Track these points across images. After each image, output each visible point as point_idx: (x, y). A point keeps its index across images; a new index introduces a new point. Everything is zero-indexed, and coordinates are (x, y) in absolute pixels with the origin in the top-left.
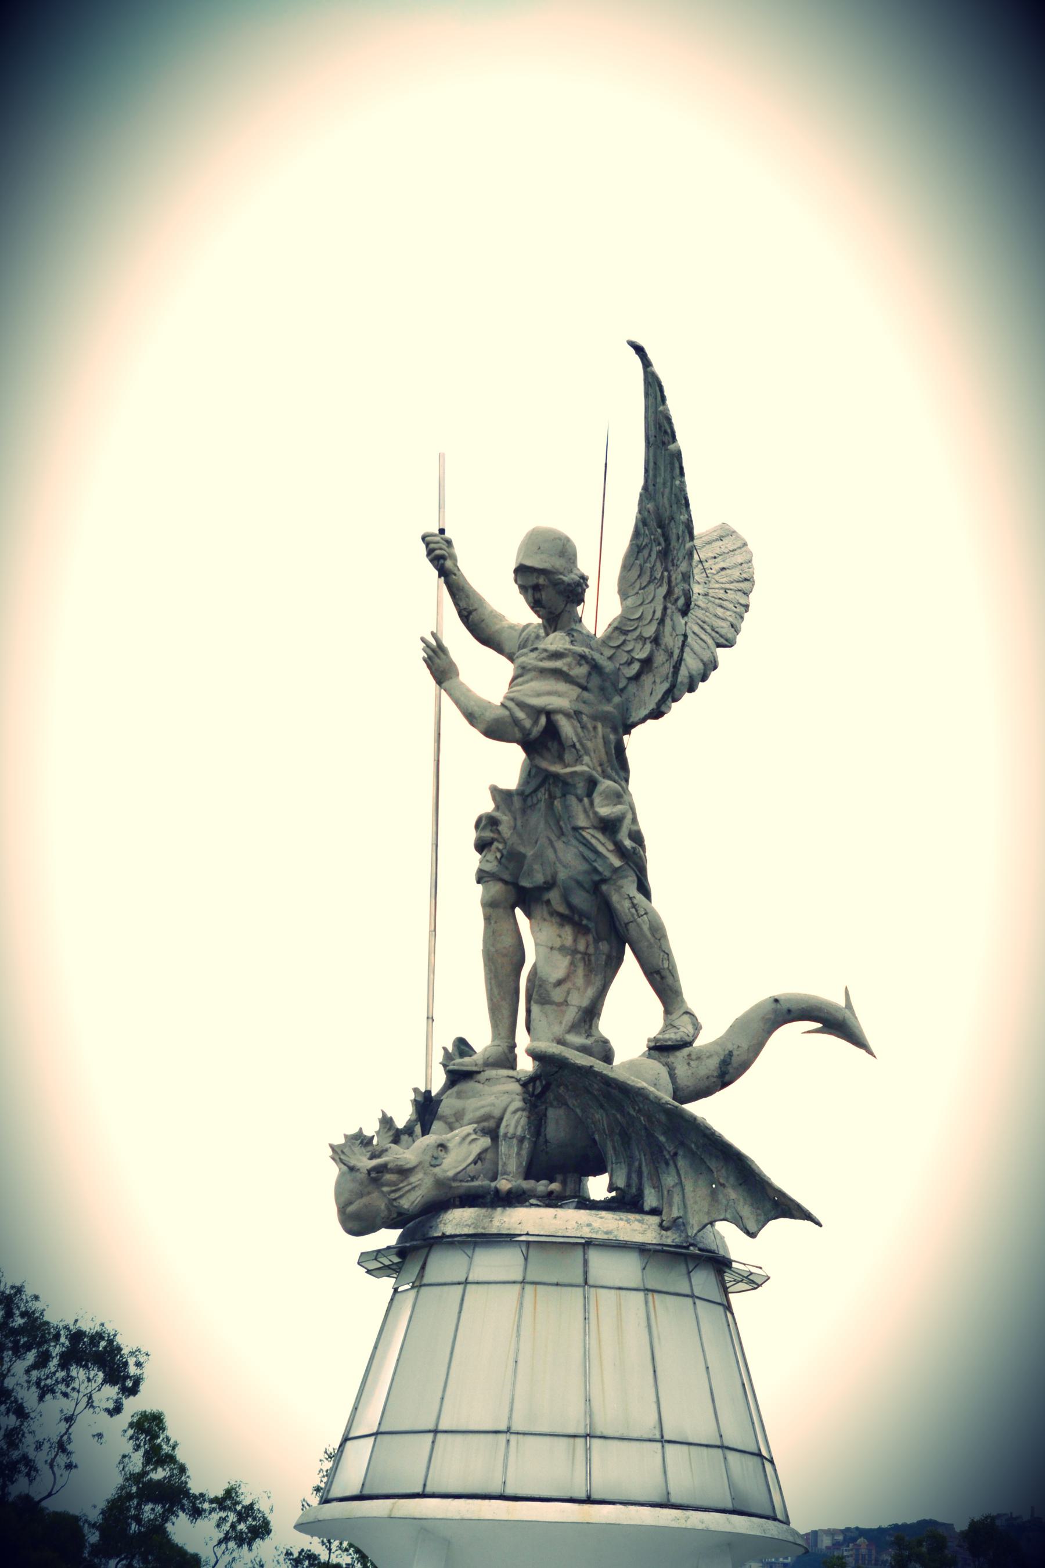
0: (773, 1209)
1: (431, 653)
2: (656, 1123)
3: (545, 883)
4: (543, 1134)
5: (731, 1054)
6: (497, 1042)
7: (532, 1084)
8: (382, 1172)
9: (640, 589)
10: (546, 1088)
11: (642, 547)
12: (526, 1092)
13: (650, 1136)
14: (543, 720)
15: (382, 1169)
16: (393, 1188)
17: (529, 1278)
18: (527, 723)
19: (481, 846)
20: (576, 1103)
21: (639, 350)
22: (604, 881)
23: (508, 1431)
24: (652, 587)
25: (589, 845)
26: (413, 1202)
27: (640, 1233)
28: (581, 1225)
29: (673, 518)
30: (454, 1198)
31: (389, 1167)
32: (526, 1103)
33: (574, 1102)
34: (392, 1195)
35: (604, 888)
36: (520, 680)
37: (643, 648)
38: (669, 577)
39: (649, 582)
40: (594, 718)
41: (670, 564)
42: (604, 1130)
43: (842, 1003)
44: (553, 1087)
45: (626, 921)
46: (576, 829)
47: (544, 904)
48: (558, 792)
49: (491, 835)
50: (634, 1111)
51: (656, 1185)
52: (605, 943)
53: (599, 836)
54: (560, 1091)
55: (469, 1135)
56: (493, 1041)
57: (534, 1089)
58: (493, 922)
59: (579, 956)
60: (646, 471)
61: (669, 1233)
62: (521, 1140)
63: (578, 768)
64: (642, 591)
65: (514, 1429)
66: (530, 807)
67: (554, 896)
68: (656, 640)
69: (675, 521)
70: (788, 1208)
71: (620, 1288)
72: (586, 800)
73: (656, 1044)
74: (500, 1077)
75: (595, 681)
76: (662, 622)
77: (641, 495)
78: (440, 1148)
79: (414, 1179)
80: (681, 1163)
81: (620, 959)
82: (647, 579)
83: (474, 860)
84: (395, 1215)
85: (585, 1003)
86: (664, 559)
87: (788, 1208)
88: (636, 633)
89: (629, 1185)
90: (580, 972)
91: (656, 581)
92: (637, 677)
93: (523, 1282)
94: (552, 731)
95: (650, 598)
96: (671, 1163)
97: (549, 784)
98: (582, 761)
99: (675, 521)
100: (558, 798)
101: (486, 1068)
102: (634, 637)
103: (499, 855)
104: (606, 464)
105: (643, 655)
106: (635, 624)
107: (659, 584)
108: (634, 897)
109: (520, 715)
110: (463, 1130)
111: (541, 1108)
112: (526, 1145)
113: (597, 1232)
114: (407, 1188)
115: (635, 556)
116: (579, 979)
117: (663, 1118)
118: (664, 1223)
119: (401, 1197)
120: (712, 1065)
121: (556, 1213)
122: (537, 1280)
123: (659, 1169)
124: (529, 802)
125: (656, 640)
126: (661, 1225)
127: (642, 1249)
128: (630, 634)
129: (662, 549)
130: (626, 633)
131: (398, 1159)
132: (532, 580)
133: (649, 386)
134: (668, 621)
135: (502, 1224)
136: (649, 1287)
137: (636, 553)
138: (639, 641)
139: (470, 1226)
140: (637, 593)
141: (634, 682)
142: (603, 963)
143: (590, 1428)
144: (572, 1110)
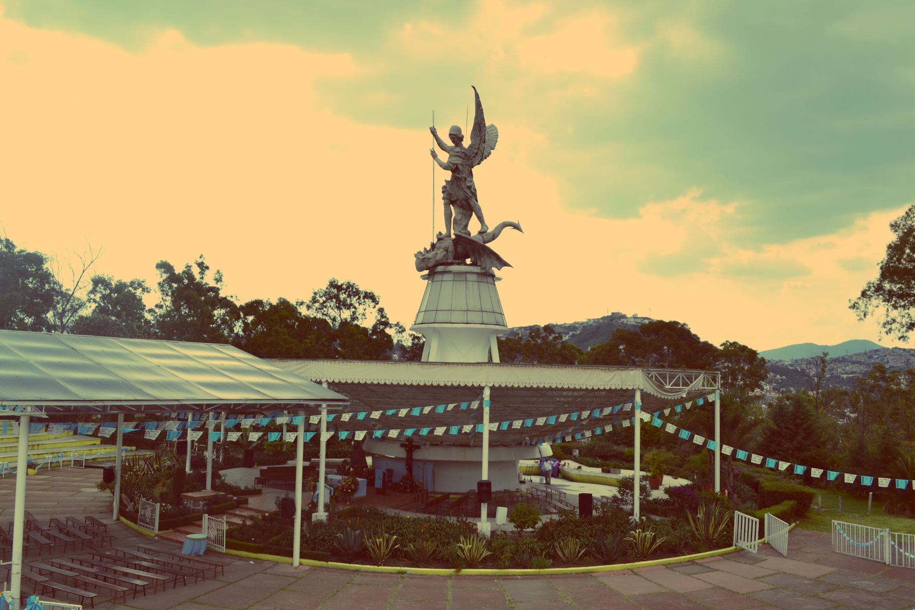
5: (495, 234)
10: (457, 242)
14: (455, 166)
15: (424, 258)
18: (452, 167)
21: (474, 88)
22: (468, 199)
23: (451, 310)
40: (466, 165)
46: (463, 188)
62: (453, 252)
63: (463, 176)
65: (453, 309)
67: (458, 202)
68: (478, 149)
70: (506, 264)
75: (466, 157)
76: (479, 145)
79: (431, 260)
81: (472, 215)
85: (465, 224)
87: (506, 264)
90: (464, 217)
92: (474, 156)
93: (454, 281)
94: (457, 168)
109: (450, 165)
112: (453, 254)
116: (464, 219)
120: (491, 235)
125: (478, 149)
127: (477, 273)
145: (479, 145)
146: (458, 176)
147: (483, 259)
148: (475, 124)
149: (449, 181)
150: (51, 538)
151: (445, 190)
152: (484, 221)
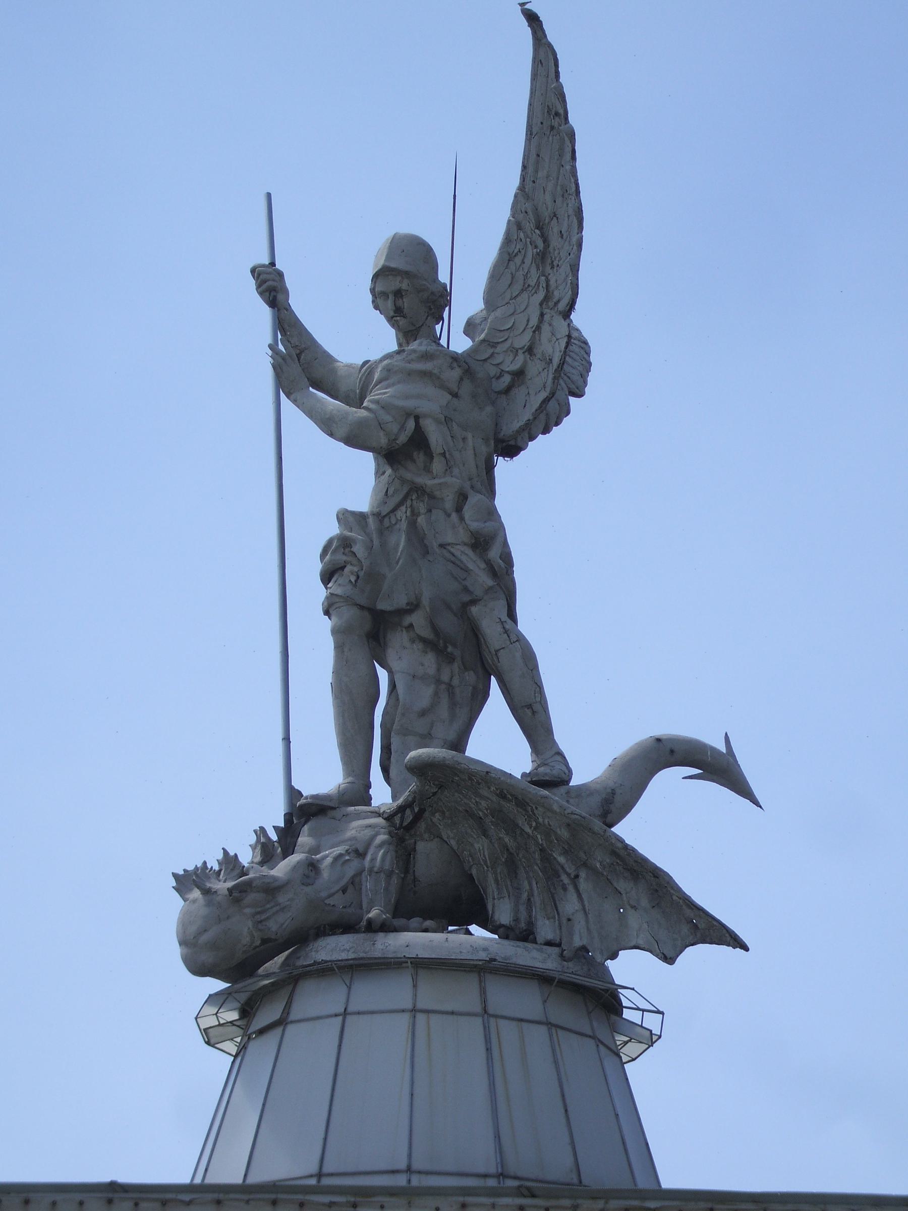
0: (692, 933)
1: (280, 360)
2: (556, 841)
3: (408, 604)
4: (411, 871)
5: (613, 792)
6: (350, 779)
7: (399, 815)
8: (245, 891)
9: (511, 300)
10: (418, 817)
11: (514, 254)
12: (393, 825)
13: (546, 858)
14: (411, 424)
16: (259, 909)
17: (420, 1005)
19: (327, 577)
20: (452, 835)
21: (533, 19)
22: (474, 602)
24: (525, 295)
25: (457, 562)
26: (282, 924)
27: (540, 962)
28: (476, 948)
29: (555, 215)
30: (325, 925)
31: (254, 885)
32: (392, 837)
33: (449, 832)
34: (258, 916)
35: (474, 610)
36: (384, 383)
38: (548, 281)
39: (522, 291)
41: (548, 268)
42: (485, 862)
43: (724, 750)
44: (427, 814)
47: (404, 629)
48: (422, 508)
49: (344, 558)
50: (531, 828)
52: (472, 673)
53: (469, 552)
54: (435, 820)
55: (341, 855)
56: (344, 779)
57: (402, 822)
58: (346, 650)
59: (443, 687)
60: (524, 167)
61: (570, 964)
62: (389, 875)
64: (514, 301)
66: (387, 528)
67: (417, 619)
69: (557, 218)
71: (521, 1020)
72: (454, 516)
73: (532, 779)
74: (360, 812)
75: (466, 388)
76: (538, 328)
77: (516, 196)
78: (310, 868)
79: (282, 899)
80: (583, 885)
81: (484, 695)
82: (520, 287)
83: (321, 593)
84: (258, 943)
86: (542, 263)
88: (507, 345)
89: (517, 920)
91: (530, 289)
92: (508, 390)
93: (414, 1011)
94: (419, 440)
95: (523, 307)
96: (571, 888)
97: (412, 500)
98: (451, 472)
99: (557, 218)
100: (423, 514)
101: (341, 806)
102: (505, 349)
103: (353, 579)
104: (455, 196)
105: (515, 367)
106: (506, 334)
107: (533, 291)
108: (505, 622)
110: (334, 851)
111: (409, 842)
112: (395, 880)
114: (275, 909)
115: (506, 265)
116: (443, 711)
117: (564, 833)
118: (565, 952)
119: (268, 918)
121: (447, 937)
122: (430, 1007)
123: (555, 895)
124: (386, 522)
126: (561, 955)
129: (540, 251)
130: (494, 345)
131: (265, 876)
132: (395, 283)
133: (540, 65)
134: (545, 328)
135: (387, 946)
136: (553, 1020)
137: (507, 262)
138: (509, 352)
139: (348, 951)
141: (504, 396)
142: (470, 695)
143: (502, 1167)
144: (446, 842)
145: (538, 328)
146: (423, 480)
147: (570, 905)
148: (515, 226)
149: (361, 517)
150: (606, 869)
151: (341, 558)
152: (549, 731)
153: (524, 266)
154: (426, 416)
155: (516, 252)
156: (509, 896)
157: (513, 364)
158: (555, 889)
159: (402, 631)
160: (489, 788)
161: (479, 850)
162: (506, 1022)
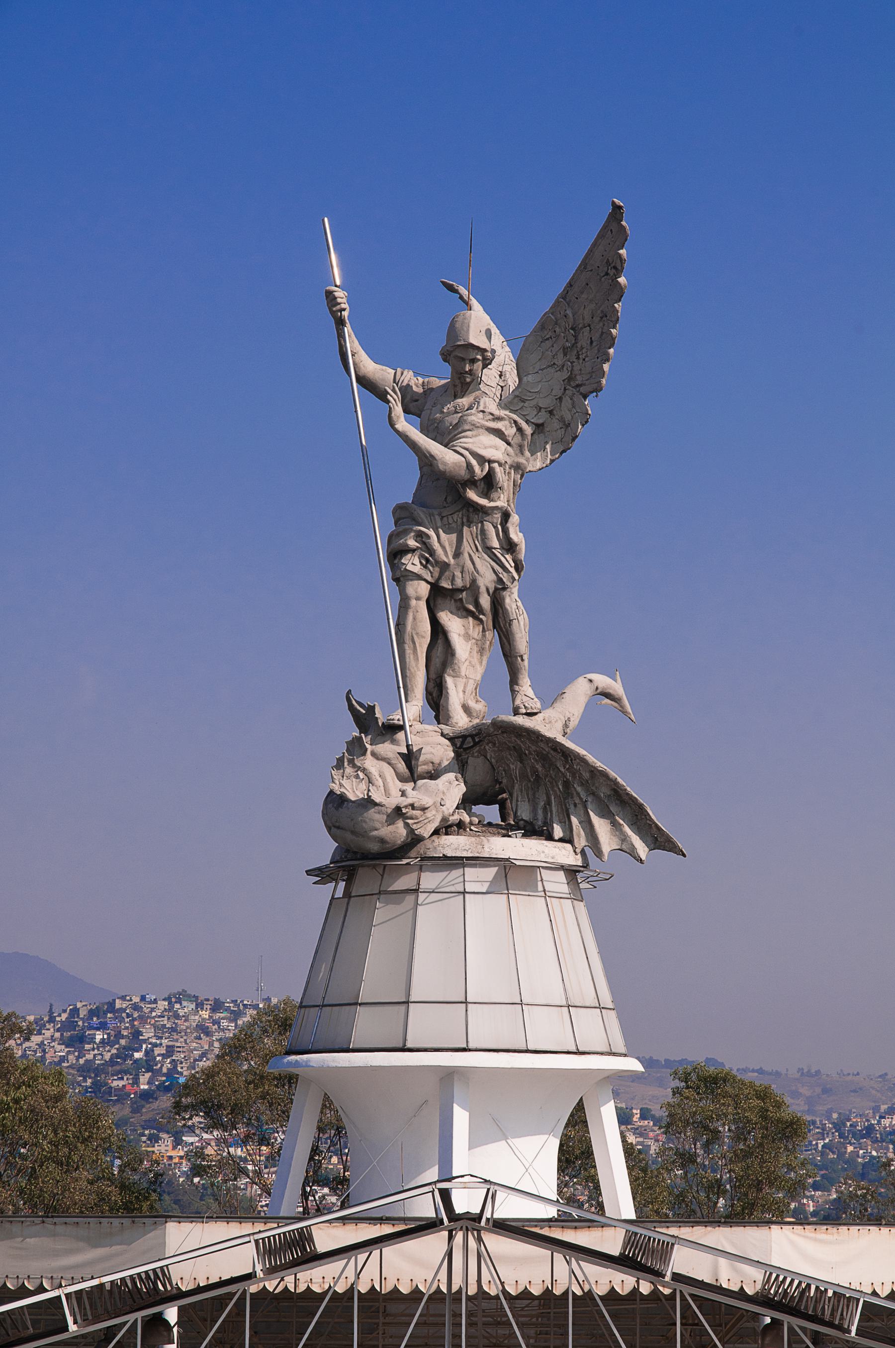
16: (416, 821)
25: (498, 562)
31: (415, 805)
37: (537, 414)
42: (516, 777)
45: (512, 619)
51: (563, 821)
79: (429, 814)
96: (580, 806)
107: (558, 369)
113: (548, 857)
117: (586, 775)
128: (528, 402)
130: (523, 401)
140: (537, 372)
153: (553, 349)
154: (494, 461)
155: (548, 336)
156: (529, 801)
157: (537, 417)
158: (569, 805)
159: (451, 600)
160: (548, 744)
161: (513, 769)
162: (555, 899)
